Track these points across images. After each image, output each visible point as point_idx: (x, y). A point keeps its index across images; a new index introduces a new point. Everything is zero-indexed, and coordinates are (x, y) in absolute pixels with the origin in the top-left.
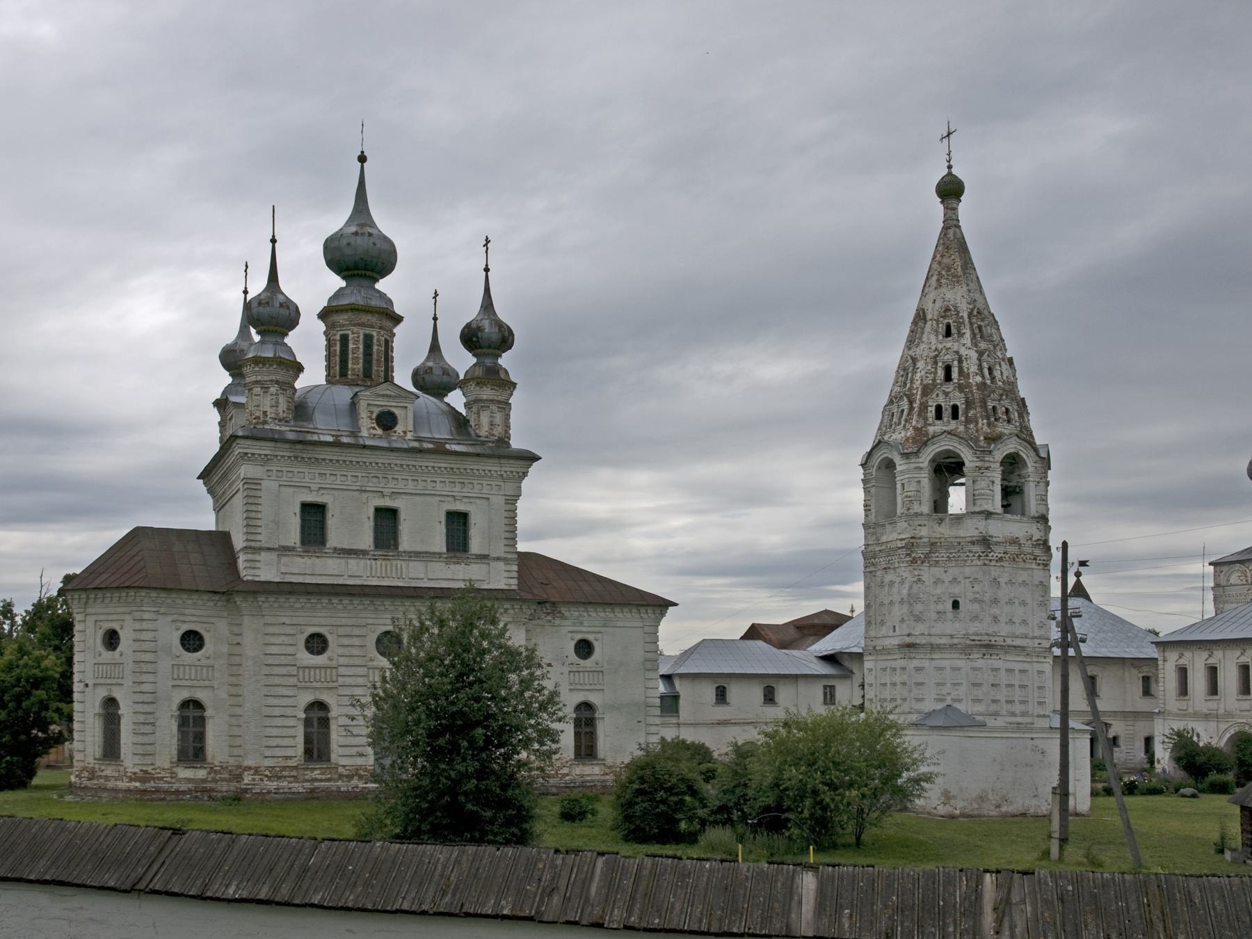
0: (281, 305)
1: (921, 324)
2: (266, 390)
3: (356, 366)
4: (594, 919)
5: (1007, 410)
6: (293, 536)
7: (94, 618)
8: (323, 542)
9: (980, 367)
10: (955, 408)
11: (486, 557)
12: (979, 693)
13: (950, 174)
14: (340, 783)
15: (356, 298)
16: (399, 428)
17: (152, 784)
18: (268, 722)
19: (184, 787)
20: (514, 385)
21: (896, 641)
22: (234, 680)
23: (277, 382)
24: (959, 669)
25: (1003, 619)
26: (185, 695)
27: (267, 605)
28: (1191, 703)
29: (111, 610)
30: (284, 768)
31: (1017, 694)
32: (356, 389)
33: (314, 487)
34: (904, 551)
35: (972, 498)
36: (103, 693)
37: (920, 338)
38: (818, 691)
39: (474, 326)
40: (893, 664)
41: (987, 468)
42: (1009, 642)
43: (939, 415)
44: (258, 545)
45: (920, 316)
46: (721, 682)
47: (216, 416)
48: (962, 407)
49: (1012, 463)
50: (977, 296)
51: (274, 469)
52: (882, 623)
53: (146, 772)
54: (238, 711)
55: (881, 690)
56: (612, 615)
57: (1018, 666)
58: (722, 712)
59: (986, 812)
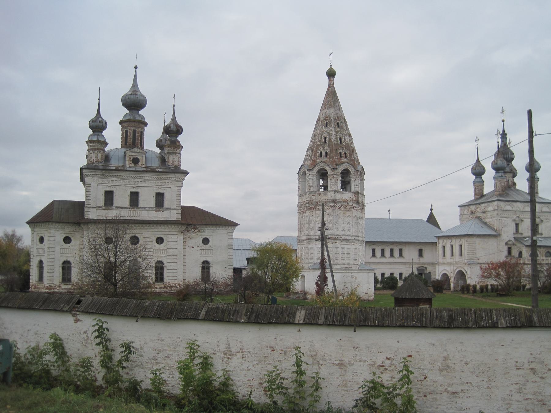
3: (130, 141)
6: (101, 203)
8: (162, 206)
9: (337, 138)
10: (326, 153)
11: (169, 209)
13: (331, 68)
16: (140, 164)
19: (63, 291)
23: (98, 149)
25: (340, 229)
26: (65, 259)
29: (41, 230)
33: (109, 185)
34: (307, 205)
36: (38, 259)
42: (343, 237)
48: (328, 152)
49: (345, 174)
53: (51, 286)
57: (346, 247)
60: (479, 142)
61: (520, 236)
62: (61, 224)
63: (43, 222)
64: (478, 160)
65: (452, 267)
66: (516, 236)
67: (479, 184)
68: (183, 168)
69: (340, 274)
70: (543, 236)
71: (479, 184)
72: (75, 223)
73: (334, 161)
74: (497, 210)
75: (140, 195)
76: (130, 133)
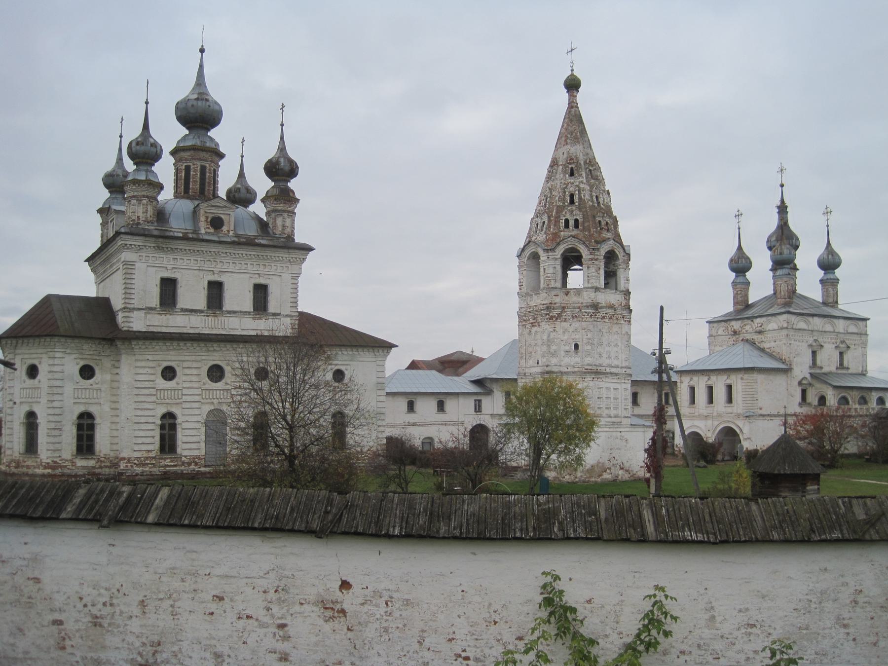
0: (152, 145)
2: (140, 202)
3: (194, 186)
6: (154, 300)
7: (21, 356)
9: (591, 196)
11: (279, 314)
13: (572, 75)
14: (183, 468)
15: (197, 142)
16: (225, 228)
17: (60, 470)
18: (137, 427)
19: (80, 472)
20: (298, 200)
22: (114, 398)
23: (147, 197)
25: (604, 355)
26: (82, 409)
27: (137, 347)
29: (32, 351)
30: (147, 458)
32: (196, 203)
35: (588, 278)
36: (26, 408)
38: (470, 403)
39: (274, 160)
42: (608, 370)
44: (132, 306)
45: (554, 163)
46: (411, 398)
47: (99, 219)
48: (580, 220)
49: (611, 257)
50: (589, 151)
51: (144, 255)
54: (116, 420)
57: (612, 386)
58: (441, 417)
61: (818, 371)
62: (77, 341)
63: (39, 336)
64: (740, 248)
65: (709, 422)
66: (812, 371)
67: (743, 286)
68: (299, 239)
70: (850, 371)
71: (741, 286)
72: (104, 339)
73: (591, 236)
74: (787, 328)
75: (226, 287)
76: (195, 171)
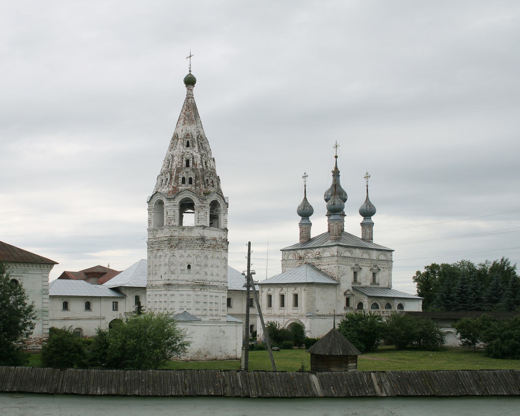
1: (176, 140)
4: (245, 395)
5: (213, 181)
10: (191, 179)
12: (198, 306)
13: (190, 74)
21: (162, 282)
24: (189, 295)
25: (209, 273)
28: (273, 310)
31: (214, 307)
34: (167, 242)
37: (176, 147)
40: (160, 293)
41: (204, 207)
42: (211, 283)
43: (183, 182)
45: (176, 137)
46: (65, 300)
48: (194, 179)
49: (214, 205)
52: (156, 274)
55: (155, 305)
56: (28, 268)
57: (214, 294)
58: (88, 314)
59: (200, 359)
60: (369, 179)
66: (354, 286)
69: (208, 327)
70: (380, 286)
